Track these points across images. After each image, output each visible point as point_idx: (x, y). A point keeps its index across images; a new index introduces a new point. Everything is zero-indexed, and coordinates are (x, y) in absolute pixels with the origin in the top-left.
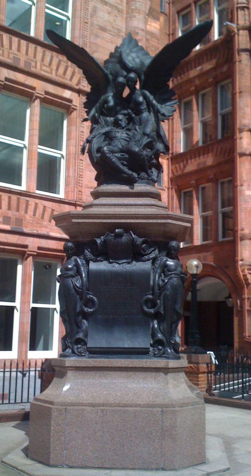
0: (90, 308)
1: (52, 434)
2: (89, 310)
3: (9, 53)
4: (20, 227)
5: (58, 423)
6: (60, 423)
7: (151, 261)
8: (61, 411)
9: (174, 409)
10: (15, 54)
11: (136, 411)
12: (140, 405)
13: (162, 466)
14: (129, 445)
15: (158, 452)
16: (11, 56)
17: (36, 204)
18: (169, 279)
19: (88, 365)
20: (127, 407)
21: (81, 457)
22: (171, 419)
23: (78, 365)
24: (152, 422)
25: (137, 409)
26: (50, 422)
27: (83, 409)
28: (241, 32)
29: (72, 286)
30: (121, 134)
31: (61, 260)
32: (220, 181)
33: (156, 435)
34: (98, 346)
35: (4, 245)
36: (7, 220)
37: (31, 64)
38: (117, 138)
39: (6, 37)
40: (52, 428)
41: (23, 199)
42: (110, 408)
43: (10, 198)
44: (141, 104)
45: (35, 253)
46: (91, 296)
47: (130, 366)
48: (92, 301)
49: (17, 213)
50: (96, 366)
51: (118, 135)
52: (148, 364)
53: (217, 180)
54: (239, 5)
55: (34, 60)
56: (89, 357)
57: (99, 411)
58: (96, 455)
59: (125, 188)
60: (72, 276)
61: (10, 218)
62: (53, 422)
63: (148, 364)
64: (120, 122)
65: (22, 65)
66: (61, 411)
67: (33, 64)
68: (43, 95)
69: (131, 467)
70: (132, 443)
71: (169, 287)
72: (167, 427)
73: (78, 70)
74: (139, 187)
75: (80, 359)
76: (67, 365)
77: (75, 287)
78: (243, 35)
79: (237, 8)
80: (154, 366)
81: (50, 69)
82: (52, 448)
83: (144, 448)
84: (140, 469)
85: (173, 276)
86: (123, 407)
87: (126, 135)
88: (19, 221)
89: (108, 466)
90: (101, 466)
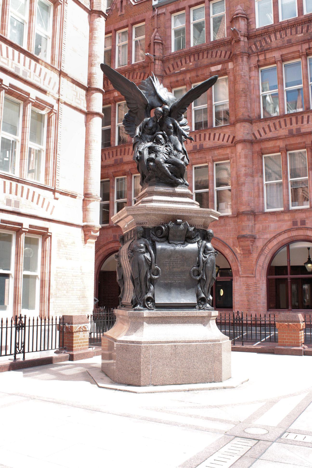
0: (156, 276)
1: (142, 364)
2: (155, 277)
3: (12, 62)
4: (18, 208)
5: (145, 356)
6: (147, 356)
7: (197, 243)
8: (147, 347)
9: (220, 343)
10: (16, 65)
11: (197, 345)
12: (198, 341)
13: (213, 380)
14: (193, 368)
15: (211, 371)
16: (14, 66)
17: (28, 190)
18: (209, 256)
19: (158, 316)
20: (190, 342)
21: (162, 378)
22: (219, 349)
23: (151, 316)
24: (207, 351)
25: (197, 343)
26: (140, 355)
27: (162, 346)
28: (157, 62)
29: (144, 259)
30: (162, 148)
31: (16, 232)
32: (133, 176)
33: (210, 360)
34: (162, 302)
35: (6, 223)
36: (9, 202)
37: (27, 73)
38: (161, 152)
39: (4, 46)
40: (142, 360)
41: (20, 185)
42: (180, 344)
43: (11, 183)
44: (171, 128)
45: (27, 230)
46: (157, 267)
47: (186, 315)
48: (158, 270)
49: (15, 197)
50: (164, 316)
51: (161, 149)
52: (197, 314)
53: (132, 174)
54: (156, 41)
55: (29, 70)
56: (156, 310)
57: (173, 346)
58: (172, 376)
59: (169, 190)
60: (144, 253)
61: (11, 200)
62: (142, 356)
63: (197, 314)
64: (161, 140)
65: (21, 75)
66: (147, 347)
67: (28, 74)
68: (34, 100)
69: (194, 382)
70: (195, 367)
71: (209, 261)
72: (216, 354)
73: (19, 73)
74: (179, 190)
75: (151, 311)
76: (144, 316)
77: (146, 259)
78: (158, 65)
79: (154, 43)
80: (201, 315)
81: (39, 79)
82: (142, 374)
83: (202, 369)
84: (187, 384)
85: (211, 254)
86: (188, 343)
87: (166, 151)
88: (17, 204)
89: (179, 383)
90: (175, 383)
